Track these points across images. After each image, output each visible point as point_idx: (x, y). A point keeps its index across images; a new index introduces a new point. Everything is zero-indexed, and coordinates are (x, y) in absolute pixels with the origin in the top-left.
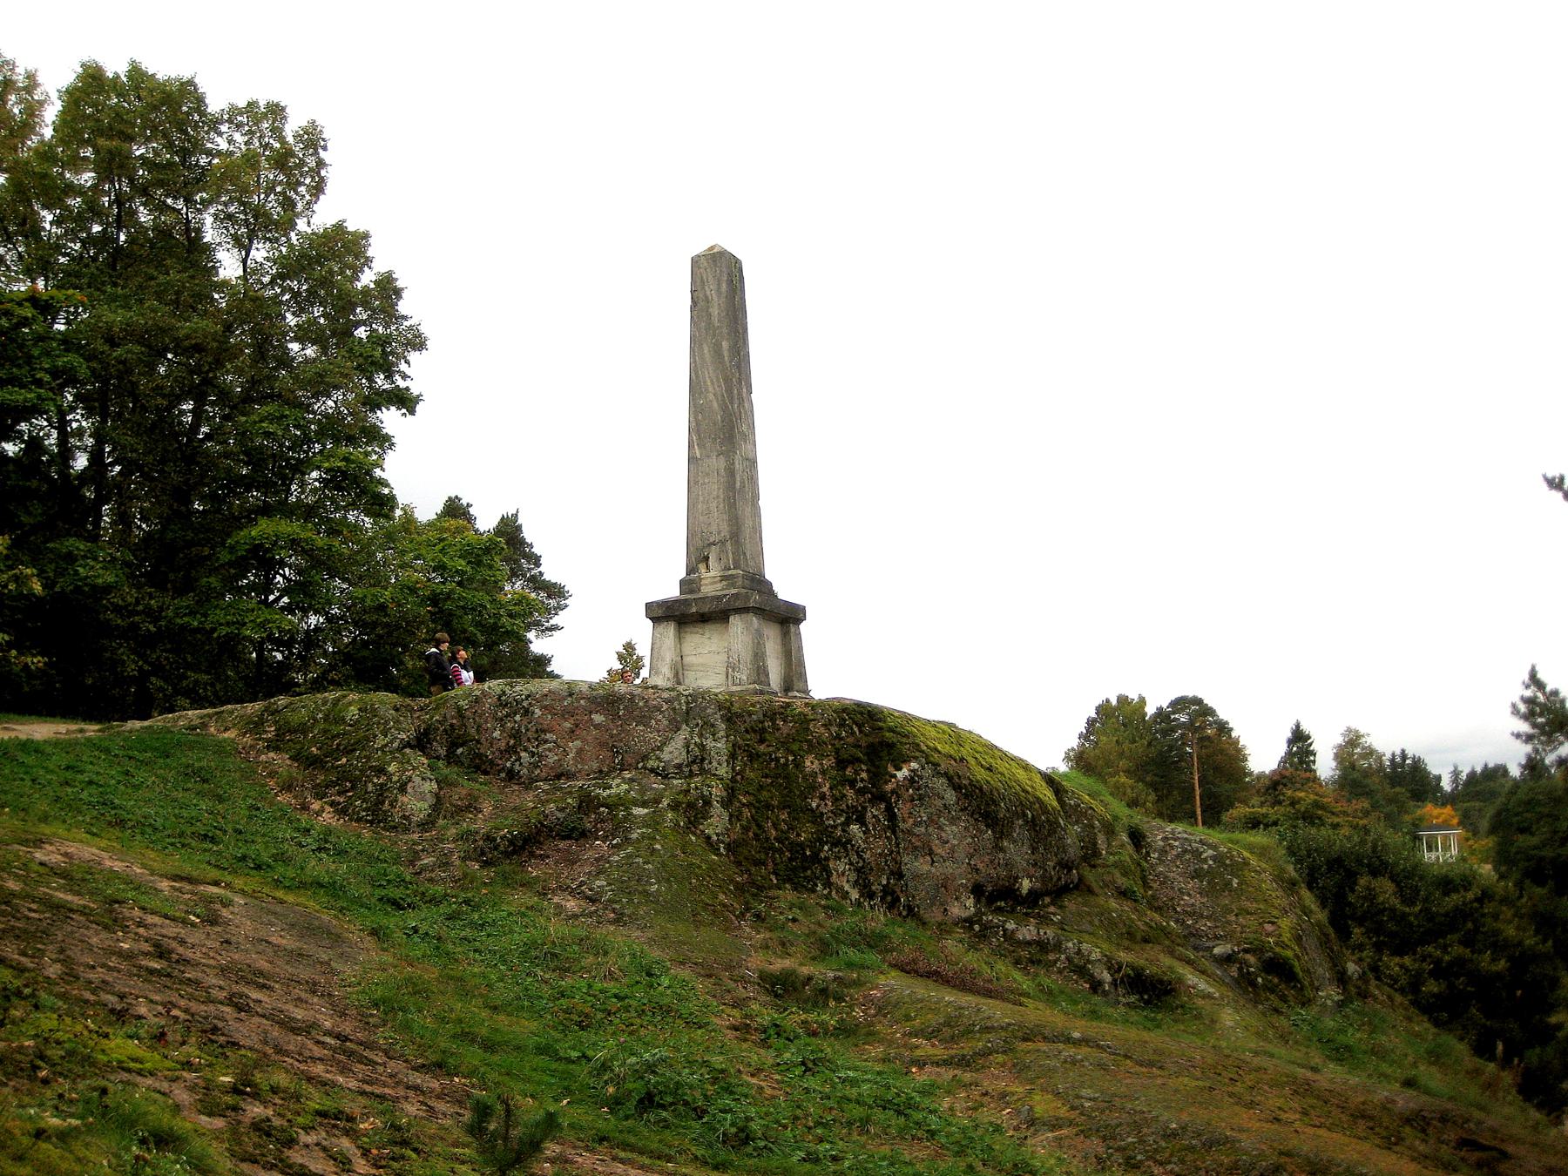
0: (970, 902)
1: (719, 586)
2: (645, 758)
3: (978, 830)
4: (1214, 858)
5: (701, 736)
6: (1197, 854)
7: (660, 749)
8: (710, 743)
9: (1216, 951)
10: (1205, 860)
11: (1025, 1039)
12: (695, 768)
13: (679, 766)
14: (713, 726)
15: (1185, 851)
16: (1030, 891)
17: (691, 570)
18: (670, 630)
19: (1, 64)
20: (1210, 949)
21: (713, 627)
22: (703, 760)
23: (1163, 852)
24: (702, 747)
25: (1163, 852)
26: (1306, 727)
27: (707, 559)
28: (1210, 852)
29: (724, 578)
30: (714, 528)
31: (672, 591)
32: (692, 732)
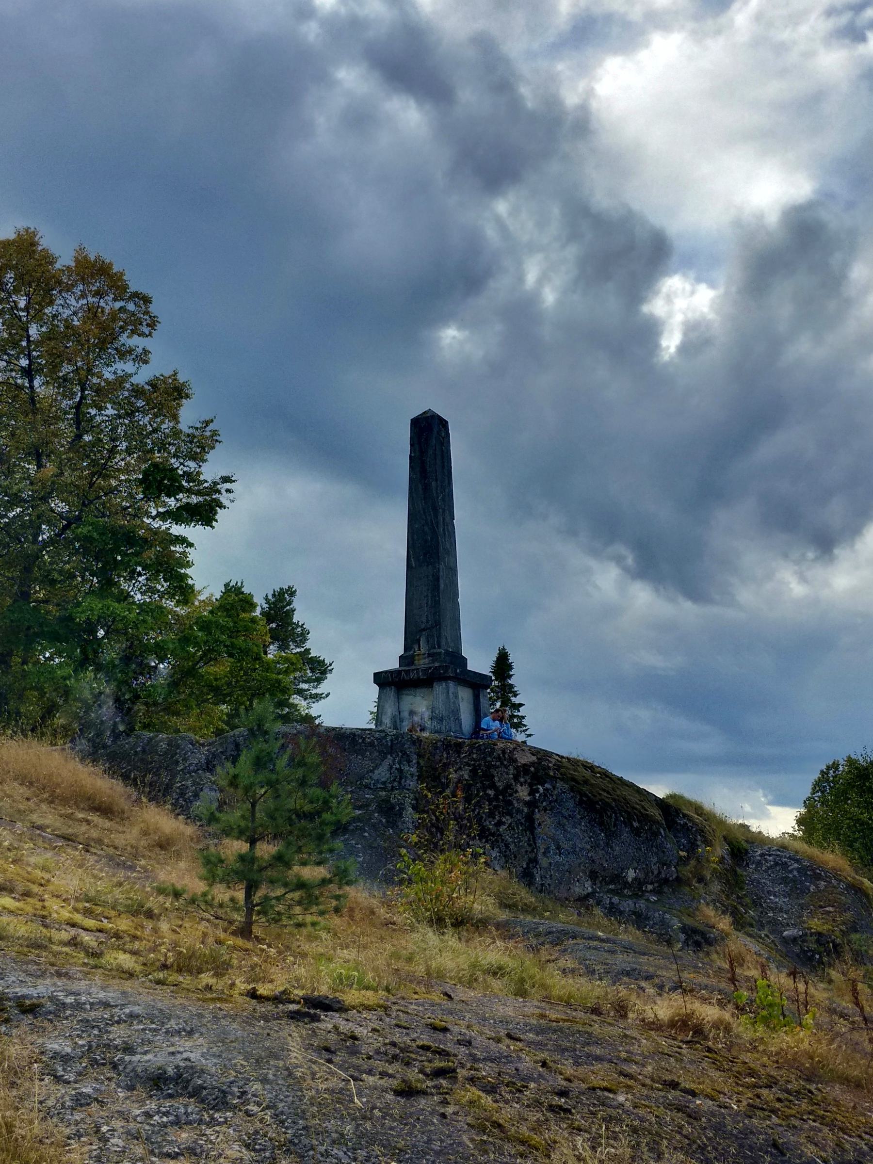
0: (588, 884)
1: (427, 661)
2: (362, 778)
3: (594, 832)
4: (798, 870)
5: (400, 763)
6: (785, 865)
7: (372, 771)
8: (406, 768)
9: (785, 933)
10: (791, 871)
11: (283, 745)
12: (396, 784)
13: (384, 783)
14: (408, 756)
15: (777, 864)
16: (635, 879)
17: (407, 648)
18: (391, 693)
19: (23, 264)
20: (782, 932)
21: (423, 690)
22: (401, 778)
23: (759, 863)
24: (400, 771)
25: (759, 863)
26: (508, 650)
27: (419, 641)
28: (796, 865)
29: (429, 655)
30: (424, 619)
31: (393, 664)
32: (394, 760)
